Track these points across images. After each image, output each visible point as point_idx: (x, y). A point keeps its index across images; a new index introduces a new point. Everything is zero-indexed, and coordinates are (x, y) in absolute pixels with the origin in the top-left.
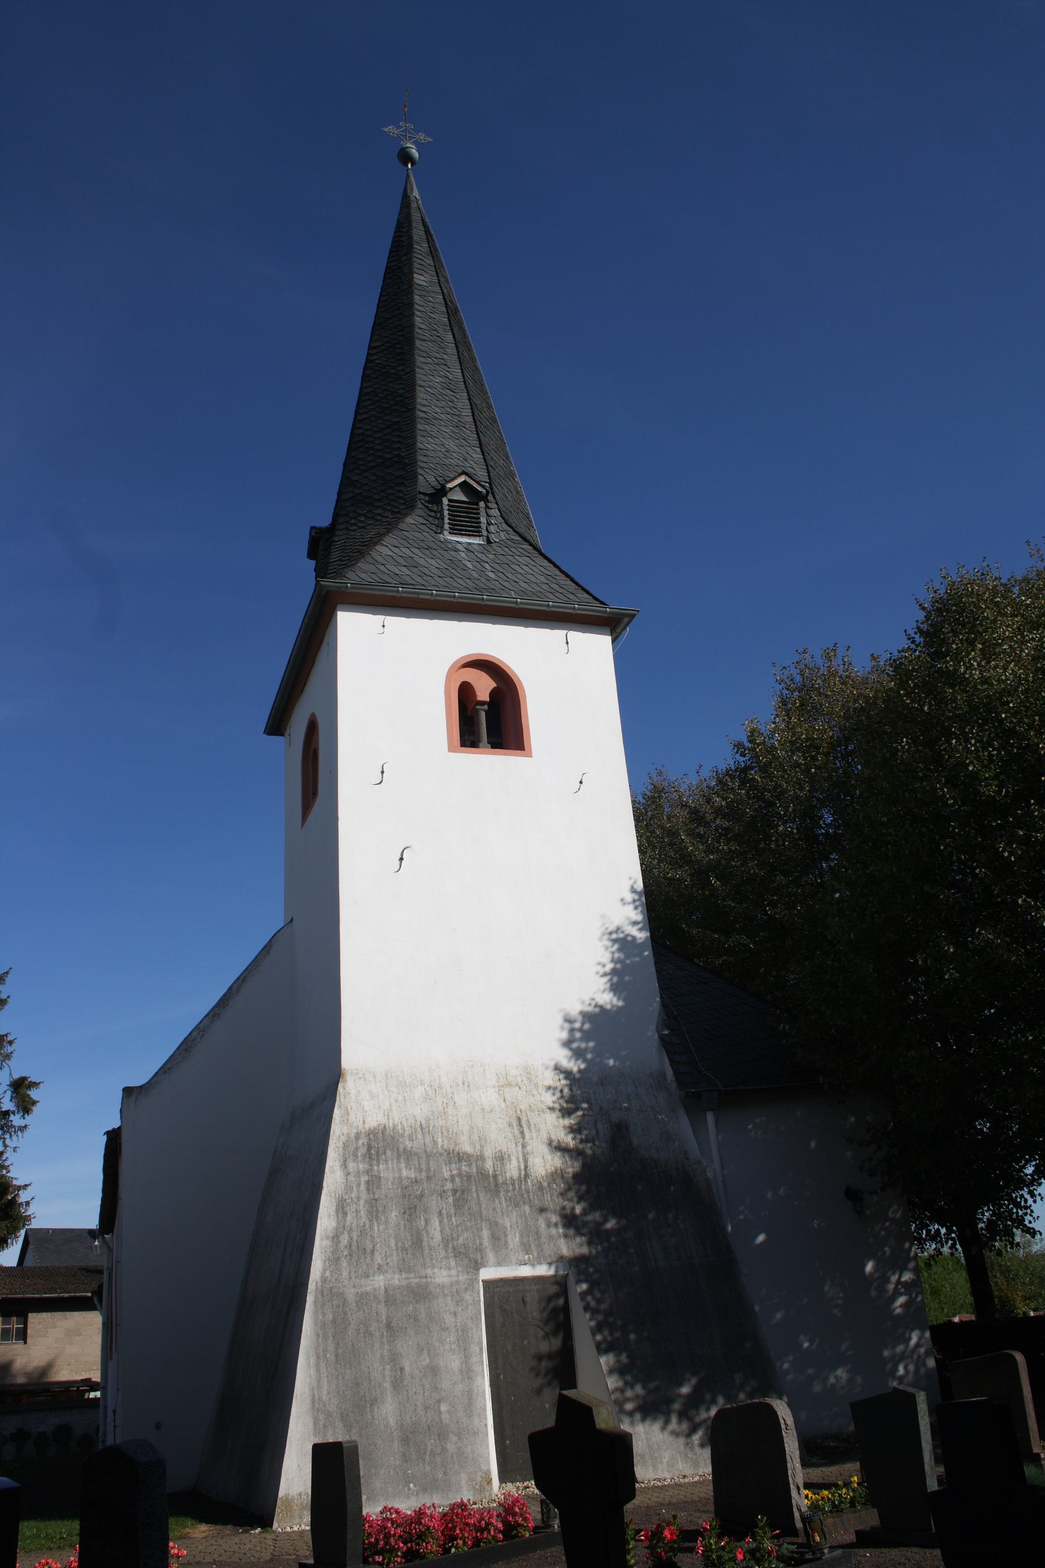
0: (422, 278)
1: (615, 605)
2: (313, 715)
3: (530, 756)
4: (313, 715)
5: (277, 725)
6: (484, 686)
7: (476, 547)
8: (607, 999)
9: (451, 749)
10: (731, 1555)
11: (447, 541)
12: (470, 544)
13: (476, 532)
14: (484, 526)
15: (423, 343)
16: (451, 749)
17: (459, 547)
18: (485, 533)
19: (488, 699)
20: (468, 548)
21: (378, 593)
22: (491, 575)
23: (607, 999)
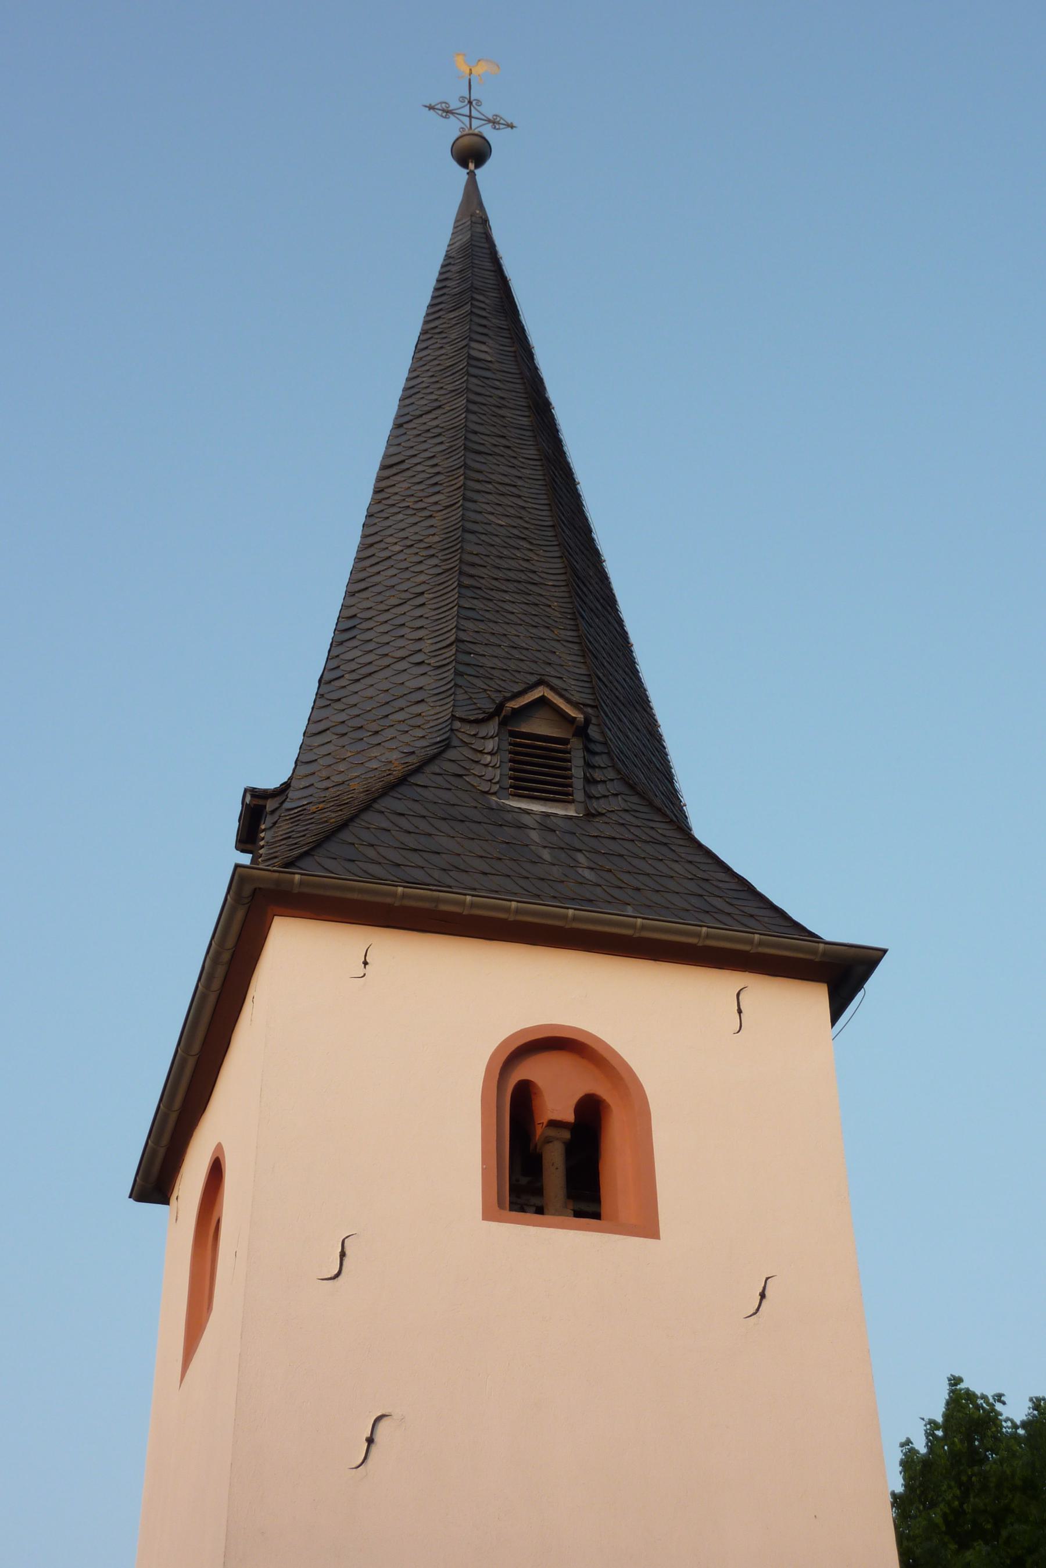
0: (483, 348)
1: (833, 925)
2: (219, 1147)
3: (647, 1227)
4: (219, 1147)
5: (155, 1183)
6: (559, 1096)
7: (560, 822)
8: (1016, 1411)
9: (487, 1216)
10: (460, 681)
11: (505, 809)
12: (547, 815)
13: (563, 796)
14: (578, 783)
15: (479, 458)
16: (487, 1216)
17: (526, 820)
18: (579, 796)
19: (569, 1117)
20: (546, 823)
21: (355, 896)
22: (587, 873)
23: (1016, 1411)
